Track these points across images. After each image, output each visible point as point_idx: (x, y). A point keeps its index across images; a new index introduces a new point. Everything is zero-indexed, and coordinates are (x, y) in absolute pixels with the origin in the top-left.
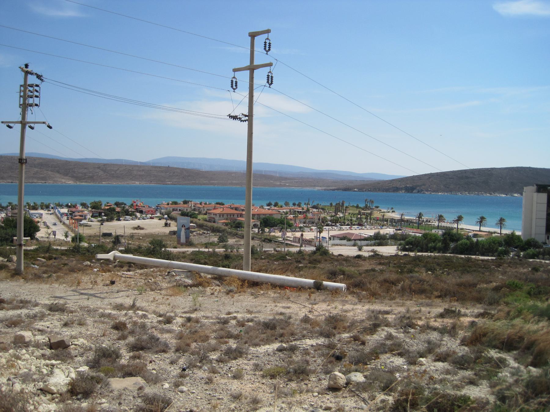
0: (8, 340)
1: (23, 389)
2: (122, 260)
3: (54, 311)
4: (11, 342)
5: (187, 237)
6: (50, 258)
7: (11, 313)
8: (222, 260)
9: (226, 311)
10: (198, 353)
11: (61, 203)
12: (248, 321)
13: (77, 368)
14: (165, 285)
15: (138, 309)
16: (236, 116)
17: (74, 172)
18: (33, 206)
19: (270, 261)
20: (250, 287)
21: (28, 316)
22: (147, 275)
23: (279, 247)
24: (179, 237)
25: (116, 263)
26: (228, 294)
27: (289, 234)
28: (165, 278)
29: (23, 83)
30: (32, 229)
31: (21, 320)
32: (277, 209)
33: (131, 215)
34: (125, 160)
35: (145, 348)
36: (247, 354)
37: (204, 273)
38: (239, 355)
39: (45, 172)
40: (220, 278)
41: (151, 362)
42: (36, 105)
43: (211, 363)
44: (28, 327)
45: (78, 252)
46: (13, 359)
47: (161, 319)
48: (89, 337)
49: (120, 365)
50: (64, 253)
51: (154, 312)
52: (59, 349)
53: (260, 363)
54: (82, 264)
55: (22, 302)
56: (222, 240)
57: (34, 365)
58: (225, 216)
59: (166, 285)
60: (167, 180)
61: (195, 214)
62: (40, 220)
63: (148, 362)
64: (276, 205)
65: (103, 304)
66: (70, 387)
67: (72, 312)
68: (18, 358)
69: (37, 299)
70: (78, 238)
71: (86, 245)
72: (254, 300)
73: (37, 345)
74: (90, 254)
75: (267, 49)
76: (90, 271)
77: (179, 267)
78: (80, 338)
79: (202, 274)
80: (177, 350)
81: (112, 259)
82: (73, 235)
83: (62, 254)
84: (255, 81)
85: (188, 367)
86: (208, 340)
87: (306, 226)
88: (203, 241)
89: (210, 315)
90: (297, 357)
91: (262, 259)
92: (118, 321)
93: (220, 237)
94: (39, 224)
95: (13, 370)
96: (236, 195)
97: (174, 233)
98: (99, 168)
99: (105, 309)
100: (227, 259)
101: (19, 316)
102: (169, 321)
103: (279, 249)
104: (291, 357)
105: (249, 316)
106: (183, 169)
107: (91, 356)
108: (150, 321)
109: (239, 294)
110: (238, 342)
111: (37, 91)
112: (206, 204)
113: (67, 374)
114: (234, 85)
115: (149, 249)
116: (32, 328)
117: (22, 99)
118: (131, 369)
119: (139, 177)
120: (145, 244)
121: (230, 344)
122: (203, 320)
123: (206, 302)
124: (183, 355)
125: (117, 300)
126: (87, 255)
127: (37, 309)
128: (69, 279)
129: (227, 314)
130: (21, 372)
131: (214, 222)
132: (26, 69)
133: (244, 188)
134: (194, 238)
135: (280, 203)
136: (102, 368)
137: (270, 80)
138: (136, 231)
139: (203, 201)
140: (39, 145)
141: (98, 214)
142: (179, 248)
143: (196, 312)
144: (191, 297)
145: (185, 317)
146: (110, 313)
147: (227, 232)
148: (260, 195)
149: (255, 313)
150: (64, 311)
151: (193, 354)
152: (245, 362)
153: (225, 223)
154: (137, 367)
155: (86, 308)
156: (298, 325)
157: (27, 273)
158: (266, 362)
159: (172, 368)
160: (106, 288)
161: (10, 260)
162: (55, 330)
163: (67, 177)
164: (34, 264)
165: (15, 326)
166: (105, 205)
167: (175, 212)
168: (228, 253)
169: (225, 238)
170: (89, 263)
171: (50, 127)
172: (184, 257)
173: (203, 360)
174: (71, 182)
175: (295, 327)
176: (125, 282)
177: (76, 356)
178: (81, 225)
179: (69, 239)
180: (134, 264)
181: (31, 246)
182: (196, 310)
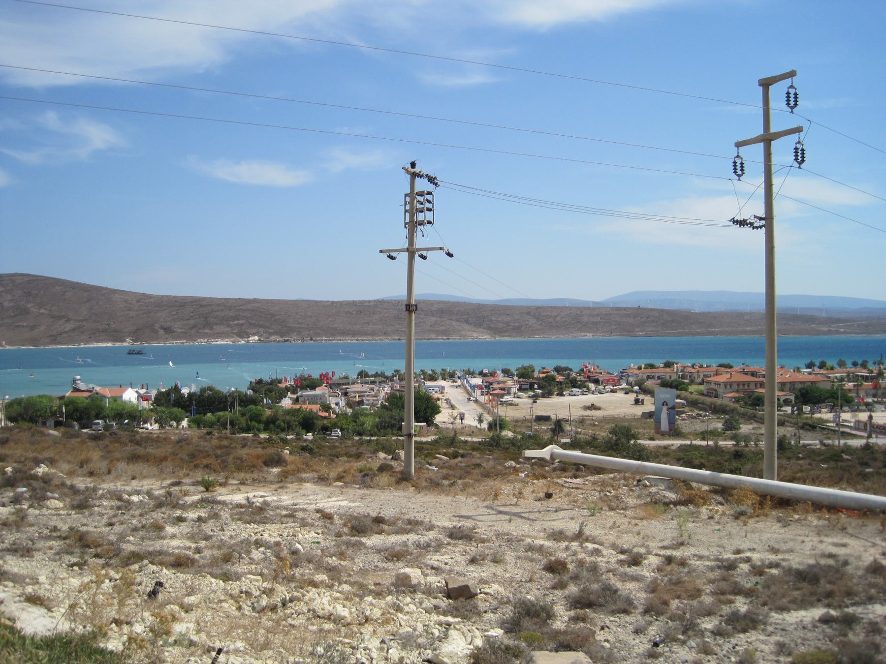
0: (387, 580)
1: (403, 657)
2: (564, 460)
3: (456, 538)
4: (392, 584)
5: (672, 422)
6: (455, 456)
7: (394, 539)
8: (729, 460)
9: (734, 548)
10: (681, 618)
11: (472, 370)
12: (771, 565)
13: (487, 631)
14: (631, 501)
15: (587, 540)
16: (745, 221)
17: (491, 321)
18: (430, 375)
19: (814, 463)
20: (776, 508)
21: (418, 545)
22: (603, 484)
23: (829, 438)
24: (658, 422)
25: (556, 465)
26: (737, 518)
27: (846, 416)
28: (632, 490)
29: (408, 192)
30: (429, 411)
31: (407, 551)
32: (825, 372)
33: (579, 387)
35: (595, 605)
36: (765, 624)
37: (698, 482)
38: (751, 625)
39: (448, 322)
40: (724, 492)
41: (602, 628)
42: (429, 222)
43: (703, 636)
44: (416, 562)
45: (498, 445)
46: (392, 611)
47: (623, 557)
48: (508, 583)
49: (553, 630)
50: (476, 447)
51: (614, 546)
52: (460, 598)
53: (787, 640)
54: (502, 464)
55: (410, 522)
56: (730, 426)
57: (421, 622)
58: (735, 387)
59: (635, 500)
60: (637, 329)
61: (683, 383)
62: (440, 396)
63: (597, 629)
64: (822, 366)
65: (533, 530)
66: (472, 661)
67: (483, 541)
68: (398, 609)
69: (433, 519)
70: (497, 424)
71: (510, 434)
72: (783, 531)
73: (429, 592)
74: (514, 449)
75: (792, 103)
76: (512, 477)
77: (655, 472)
78: (494, 584)
79: (694, 485)
80: (647, 611)
81: (548, 457)
82: (491, 419)
83: (474, 449)
84: (774, 159)
85: (662, 641)
86: (700, 596)
87: (878, 402)
88: (699, 429)
89: (705, 553)
90: (856, 636)
91: (798, 458)
92: (553, 559)
93: (726, 422)
94: (439, 403)
95: (389, 628)
96: (753, 351)
97: (650, 415)
98: (529, 313)
99: (536, 538)
100: (738, 460)
101: (405, 544)
102: (636, 561)
103: (830, 442)
104: (845, 635)
105: (773, 557)
106: (662, 311)
107: (508, 612)
108: (605, 560)
109: (757, 519)
110: (751, 602)
111: (429, 202)
112: (701, 367)
113: (470, 640)
114: (739, 169)
115: (608, 441)
116: (423, 563)
117: (408, 214)
118: (568, 637)
119: (586, 327)
120: (603, 434)
121: (738, 605)
122: (693, 562)
123: (699, 530)
124: (657, 620)
125: (555, 523)
126: (511, 450)
127: (431, 535)
128: (481, 488)
129: (734, 553)
130: (401, 631)
131: (716, 397)
132: (413, 170)
133: (762, 339)
134: (683, 423)
135: (829, 363)
136: (524, 634)
137: (800, 156)
138: (589, 413)
139: (698, 361)
140: (435, 282)
141: (528, 387)
142: (659, 439)
143: (682, 548)
144: (675, 522)
145: (664, 556)
146: (542, 546)
147: (739, 414)
148: (788, 350)
149: (784, 552)
150: (471, 540)
151: (671, 619)
152: (762, 637)
153: (734, 398)
154: (578, 636)
155: (505, 535)
156: (860, 577)
157: (419, 478)
158: (799, 641)
159: (637, 641)
160: (537, 503)
161: (396, 458)
162: (457, 568)
163: (481, 330)
164: (430, 464)
165: (398, 560)
166: (540, 372)
167: (650, 381)
168: (740, 449)
169: (734, 423)
170: (513, 463)
171: (450, 255)
172: (666, 455)
173: (688, 629)
174: (487, 337)
175: (855, 581)
176: (568, 495)
177: (485, 612)
178: (502, 403)
179: (485, 425)
180: (584, 466)
181: (428, 436)
182: (682, 544)
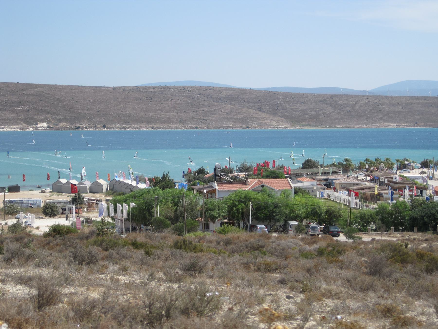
34: (343, 89)
98: (324, 101)
119: (388, 117)
174: (286, 126)
